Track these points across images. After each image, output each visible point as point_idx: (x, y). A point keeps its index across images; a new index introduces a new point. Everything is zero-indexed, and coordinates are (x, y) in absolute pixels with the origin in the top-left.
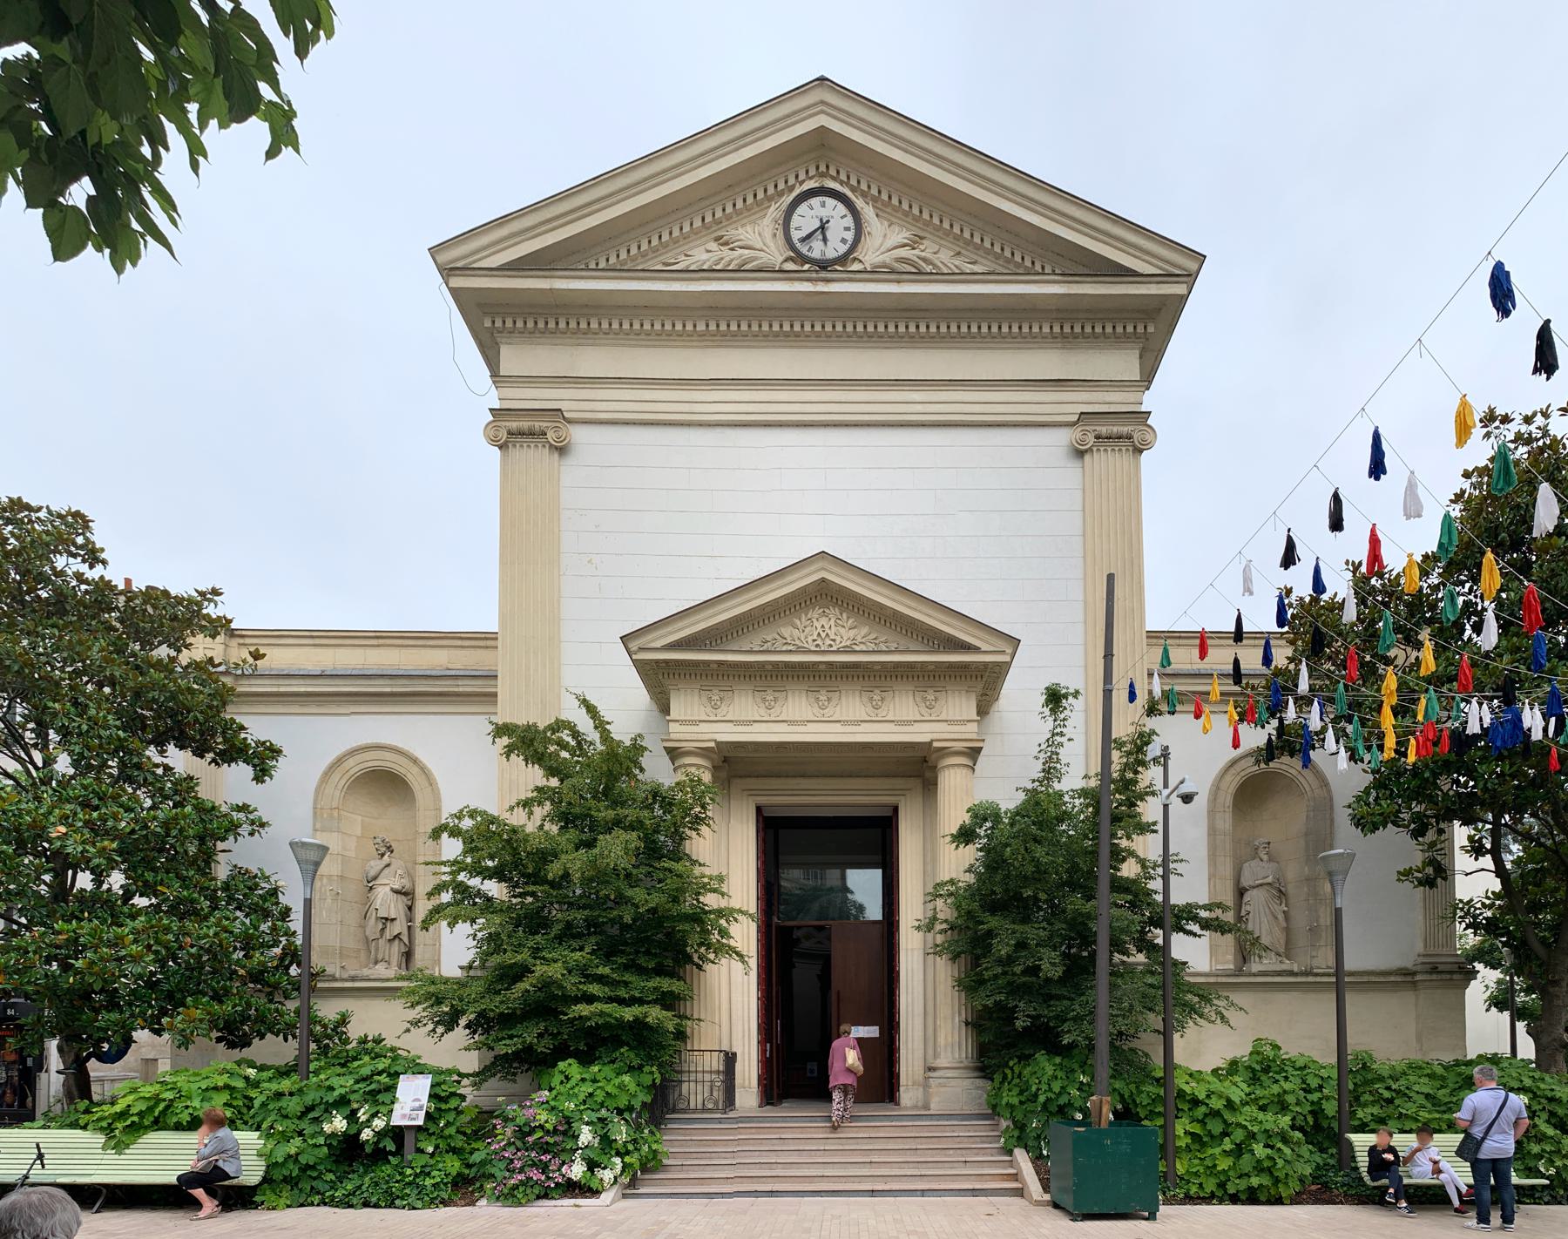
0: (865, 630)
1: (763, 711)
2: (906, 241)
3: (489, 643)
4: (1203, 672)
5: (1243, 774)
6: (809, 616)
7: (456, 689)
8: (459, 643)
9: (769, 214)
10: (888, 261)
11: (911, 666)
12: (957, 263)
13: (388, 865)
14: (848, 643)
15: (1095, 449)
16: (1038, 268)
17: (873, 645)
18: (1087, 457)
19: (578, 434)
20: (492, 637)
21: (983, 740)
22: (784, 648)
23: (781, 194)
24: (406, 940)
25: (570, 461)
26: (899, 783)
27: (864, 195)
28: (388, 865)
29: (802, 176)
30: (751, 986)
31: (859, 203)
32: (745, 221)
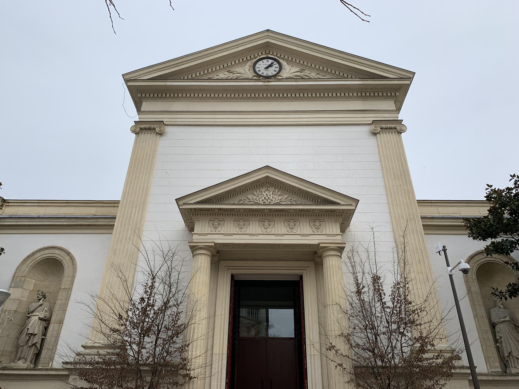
0: (285, 197)
1: (237, 230)
2: (298, 71)
3: (116, 205)
4: (445, 217)
5: (478, 263)
6: (261, 191)
7: (96, 223)
8: (102, 205)
9: (247, 64)
10: (292, 76)
11: (308, 210)
12: (318, 76)
13: (41, 305)
14: (278, 201)
15: (381, 132)
16: (345, 75)
17: (290, 202)
18: (378, 135)
19: (168, 129)
20: (117, 202)
21: (345, 243)
22: (249, 203)
23: (253, 59)
24: (39, 346)
25: (163, 138)
26: (303, 264)
27: (282, 59)
28: (41, 305)
29: (260, 54)
30: (223, 375)
31: (281, 61)
32: (239, 66)
